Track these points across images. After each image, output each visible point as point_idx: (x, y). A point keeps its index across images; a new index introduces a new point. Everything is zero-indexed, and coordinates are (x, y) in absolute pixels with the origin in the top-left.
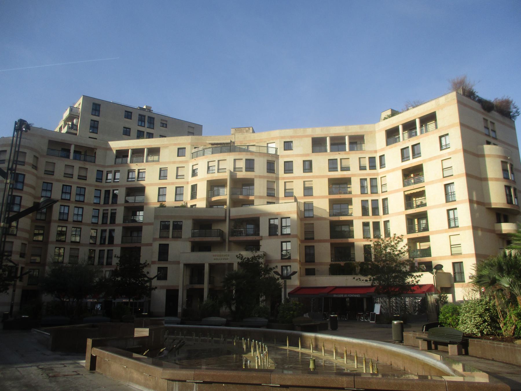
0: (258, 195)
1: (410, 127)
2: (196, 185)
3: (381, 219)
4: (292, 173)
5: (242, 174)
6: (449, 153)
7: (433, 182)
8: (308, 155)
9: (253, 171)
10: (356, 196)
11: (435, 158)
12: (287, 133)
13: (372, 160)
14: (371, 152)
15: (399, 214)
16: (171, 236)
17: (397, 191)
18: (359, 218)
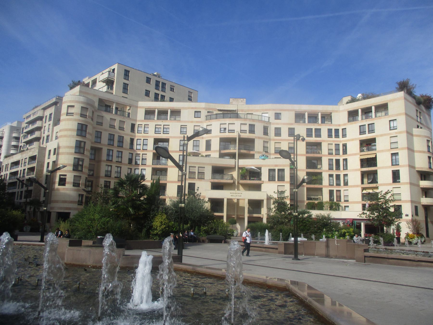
0: (257, 151)
1: (367, 111)
2: (211, 140)
3: (342, 173)
4: (281, 136)
5: (247, 135)
6: (396, 133)
7: (382, 151)
8: (292, 124)
9: (254, 133)
10: (325, 156)
11: (385, 135)
12: (278, 107)
13: (337, 131)
14: (336, 125)
15: (356, 170)
16: (196, 177)
17: (355, 154)
18: (326, 171)
